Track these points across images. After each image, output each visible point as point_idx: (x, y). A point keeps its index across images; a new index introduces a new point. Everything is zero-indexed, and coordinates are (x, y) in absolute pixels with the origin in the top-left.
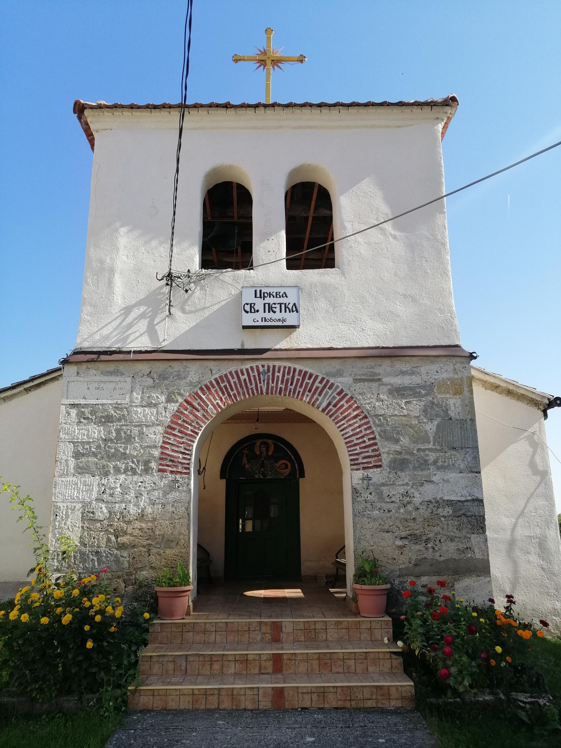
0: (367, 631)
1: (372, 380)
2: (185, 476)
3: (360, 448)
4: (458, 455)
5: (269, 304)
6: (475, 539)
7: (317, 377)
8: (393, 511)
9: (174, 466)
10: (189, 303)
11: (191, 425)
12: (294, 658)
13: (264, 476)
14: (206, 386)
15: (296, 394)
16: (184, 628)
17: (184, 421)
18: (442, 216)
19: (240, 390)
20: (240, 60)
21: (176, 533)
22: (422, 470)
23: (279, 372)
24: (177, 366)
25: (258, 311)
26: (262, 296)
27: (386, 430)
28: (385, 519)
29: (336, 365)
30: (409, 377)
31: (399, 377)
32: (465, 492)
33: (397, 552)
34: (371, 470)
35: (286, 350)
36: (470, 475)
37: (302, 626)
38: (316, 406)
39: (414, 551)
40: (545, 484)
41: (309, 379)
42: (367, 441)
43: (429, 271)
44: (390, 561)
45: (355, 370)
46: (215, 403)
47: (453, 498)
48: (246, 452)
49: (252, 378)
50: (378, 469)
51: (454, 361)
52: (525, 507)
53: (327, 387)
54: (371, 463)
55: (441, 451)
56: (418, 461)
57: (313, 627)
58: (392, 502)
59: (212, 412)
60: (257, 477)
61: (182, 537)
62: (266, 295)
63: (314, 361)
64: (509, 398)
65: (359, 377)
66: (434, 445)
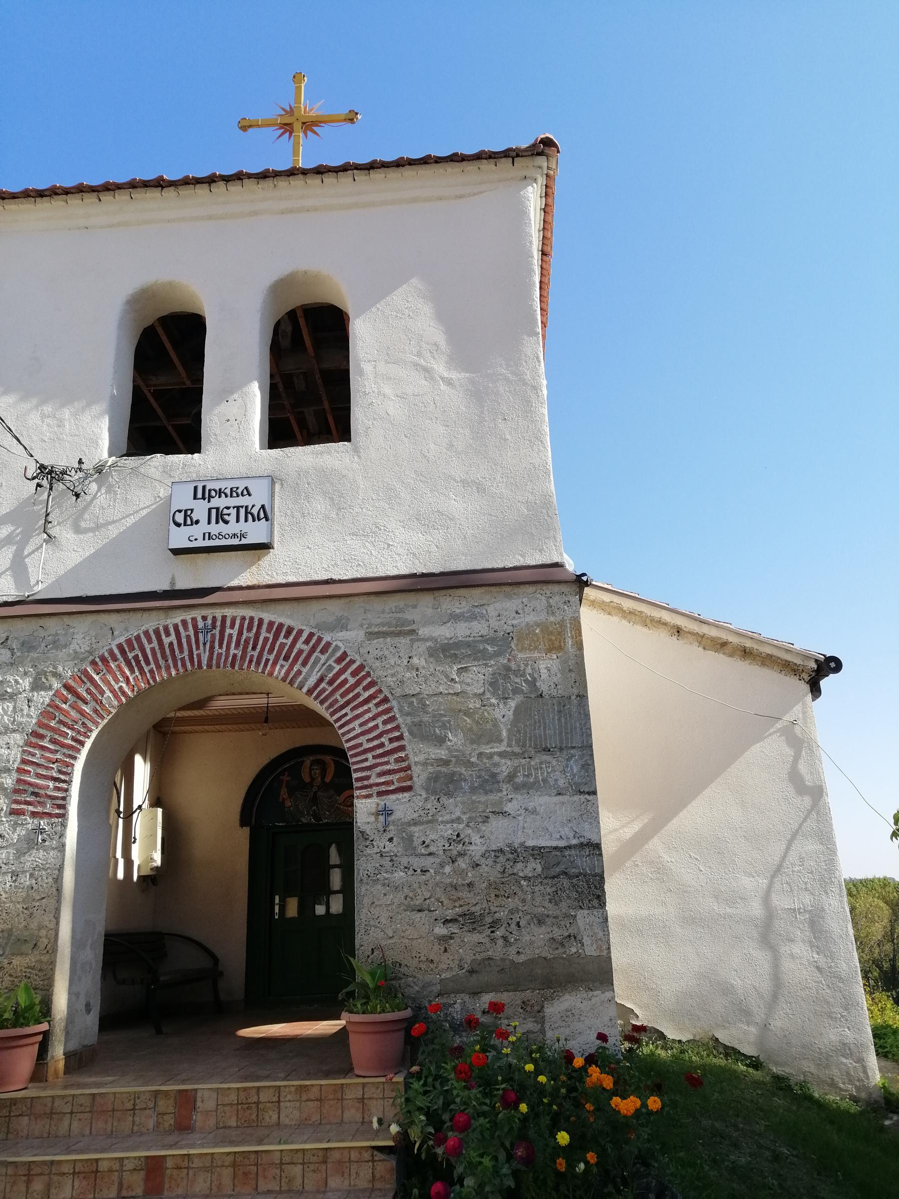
0: (357, 1105)
1: (399, 634)
2: (56, 820)
3: (374, 757)
4: (554, 763)
5: (217, 509)
6: (584, 918)
7: (300, 632)
8: (432, 871)
9: (39, 802)
10: (86, 516)
11: (73, 729)
12: (186, 1164)
13: (317, 818)
14: (103, 659)
15: (262, 664)
16: (14, 1108)
17: (61, 722)
18: (533, 339)
19: (162, 662)
20: (250, 126)
21: (34, 925)
22: (486, 793)
23: (232, 627)
24: (52, 625)
25: (197, 522)
26: (206, 495)
27: (421, 721)
28: (415, 886)
29: (335, 608)
30: (466, 624)
31: (449, 625)
32: (566, 831)
33: (436, 947)
34: (393, 797)
35: (249, 588)
36: (576, 798)
37: (233, 1098)
38: (296, 685)
39: (469, 945)
40: (818, 814)
41: (286, 637)
42: (387, 743)
43: (508, 437)
44: (423, 966)
45: (369, 616)
46: (116, 687)
47: (544, 842)
48: (286, 778)
49: (184, 641)
50: (406, 795)
51: (548, 592)
52: (784, 858)
53: (318, 650)
54: (393, 783)
55: (521, 755)
56: (480, 777)
57: (255, 1099)
58: (430, 854)
59: (110, 704)
60: (304, 820)
61: (43, 932)
62: (213, 493)
63: (295, 604)
64: (747, 662)
65: (376, 630)
66: (509, 745)
